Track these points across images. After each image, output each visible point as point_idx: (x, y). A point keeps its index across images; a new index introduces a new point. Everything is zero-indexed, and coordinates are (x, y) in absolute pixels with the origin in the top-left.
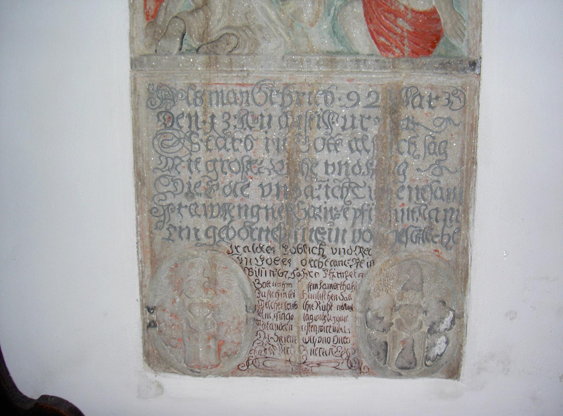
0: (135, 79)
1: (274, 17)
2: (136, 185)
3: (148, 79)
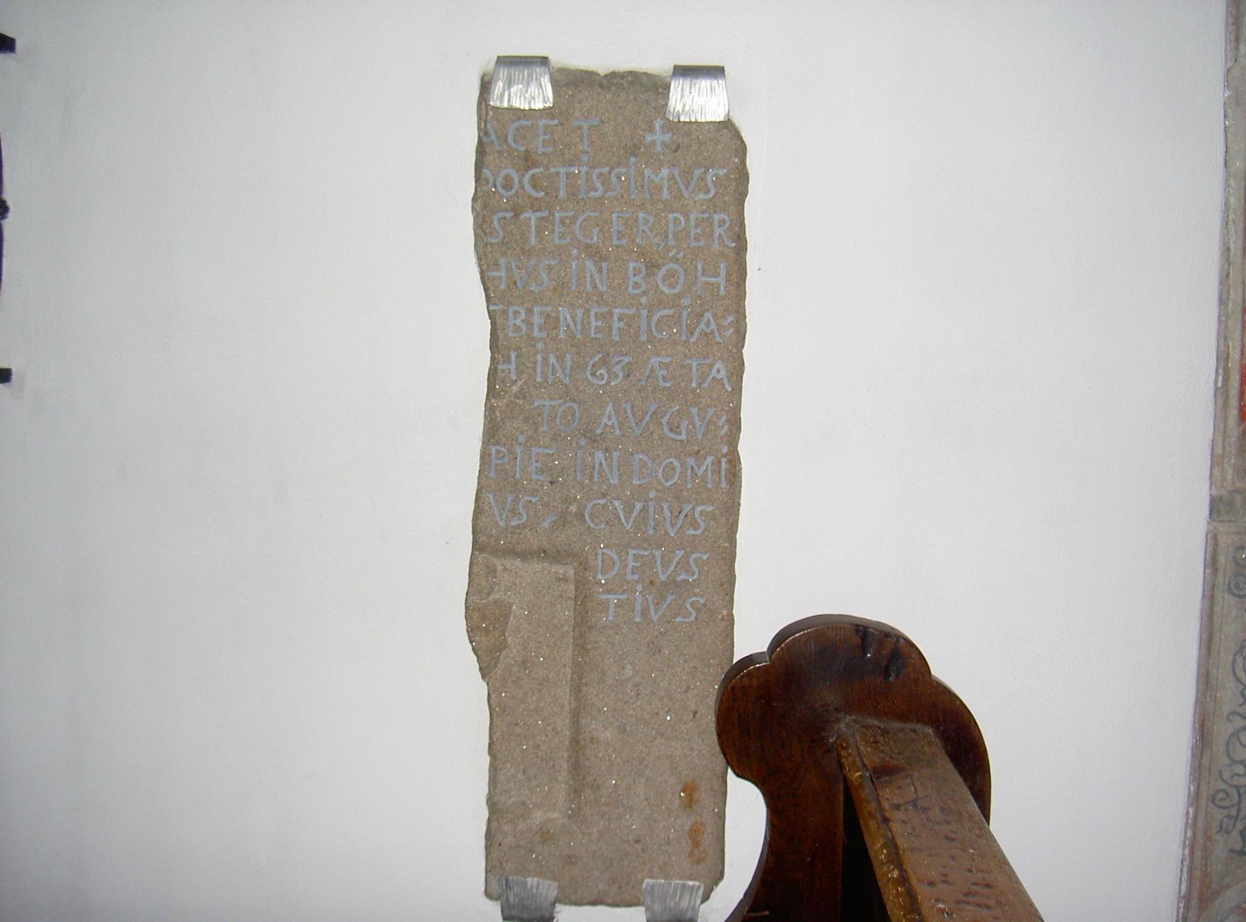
0: (1215, 538)
1: (1229, 477)
2: (1194, 748)
3: (1237, 538)
